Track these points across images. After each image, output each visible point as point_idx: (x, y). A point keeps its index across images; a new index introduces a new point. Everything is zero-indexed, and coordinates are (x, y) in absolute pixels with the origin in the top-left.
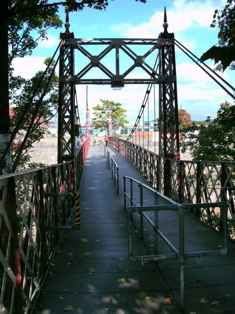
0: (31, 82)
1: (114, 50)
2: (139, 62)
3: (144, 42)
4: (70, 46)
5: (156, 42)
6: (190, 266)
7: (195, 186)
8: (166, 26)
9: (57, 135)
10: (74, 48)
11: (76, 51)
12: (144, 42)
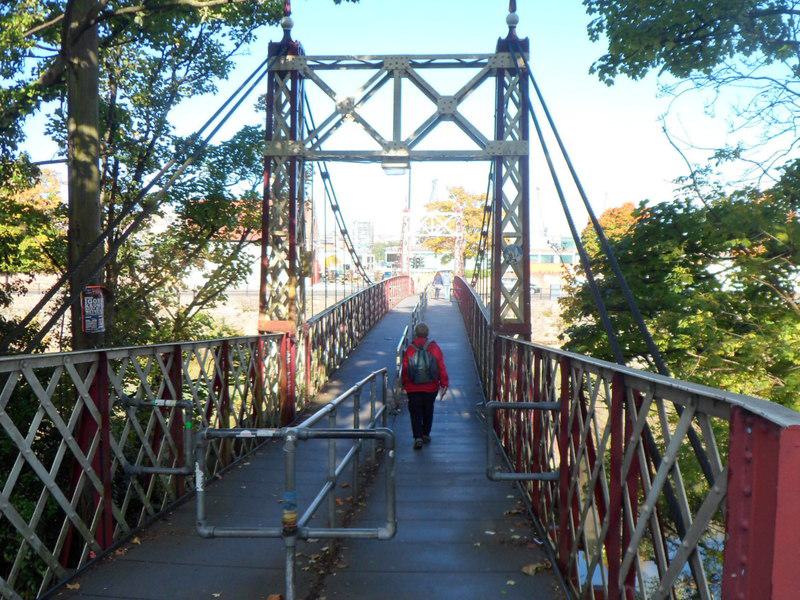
0: (219, 181)
1: (391, 82)
2: (447, 110)
3: (460, 63)
4: (289, 75)
5: (486, 61)
6: (393, 568)
7: (231, 418)
8: (512, 23)
9: (532, 292)
10: (301, 78)
11: (308, 84)
12: (460, 63)
